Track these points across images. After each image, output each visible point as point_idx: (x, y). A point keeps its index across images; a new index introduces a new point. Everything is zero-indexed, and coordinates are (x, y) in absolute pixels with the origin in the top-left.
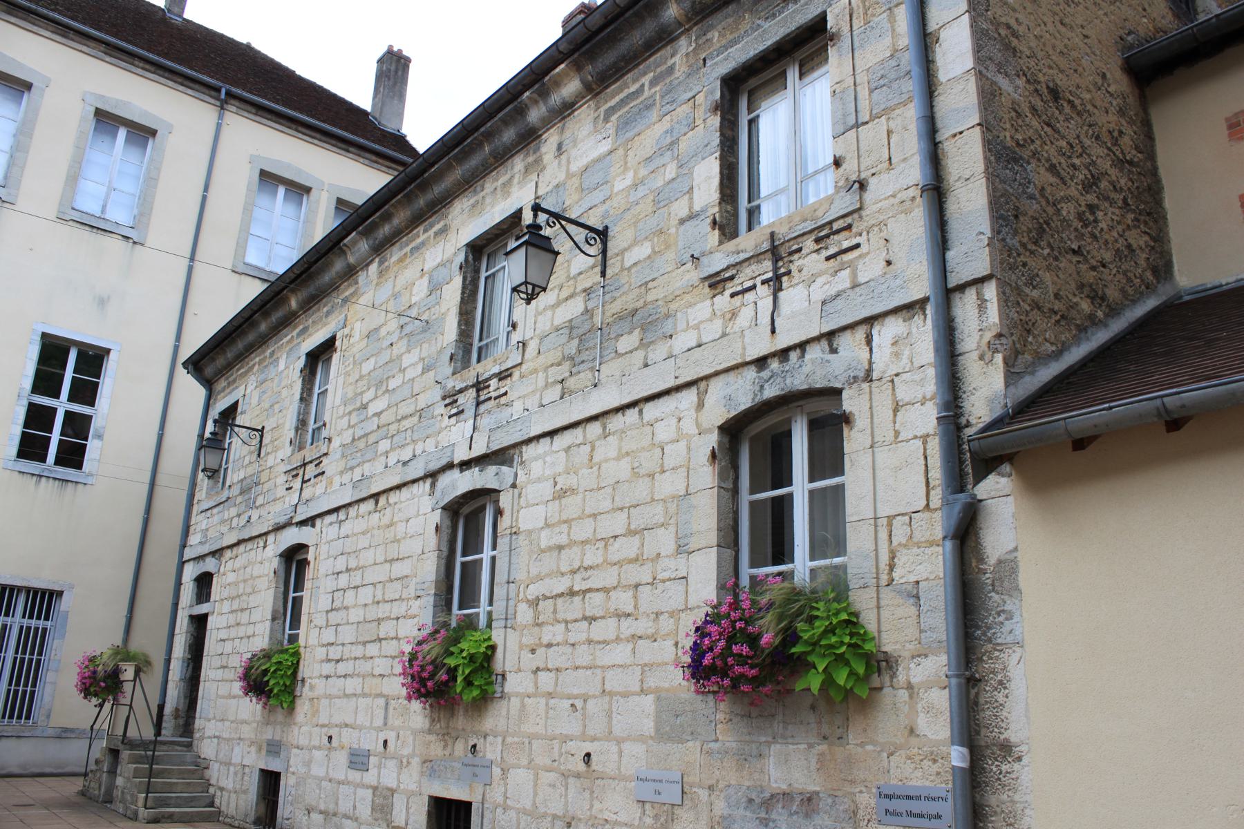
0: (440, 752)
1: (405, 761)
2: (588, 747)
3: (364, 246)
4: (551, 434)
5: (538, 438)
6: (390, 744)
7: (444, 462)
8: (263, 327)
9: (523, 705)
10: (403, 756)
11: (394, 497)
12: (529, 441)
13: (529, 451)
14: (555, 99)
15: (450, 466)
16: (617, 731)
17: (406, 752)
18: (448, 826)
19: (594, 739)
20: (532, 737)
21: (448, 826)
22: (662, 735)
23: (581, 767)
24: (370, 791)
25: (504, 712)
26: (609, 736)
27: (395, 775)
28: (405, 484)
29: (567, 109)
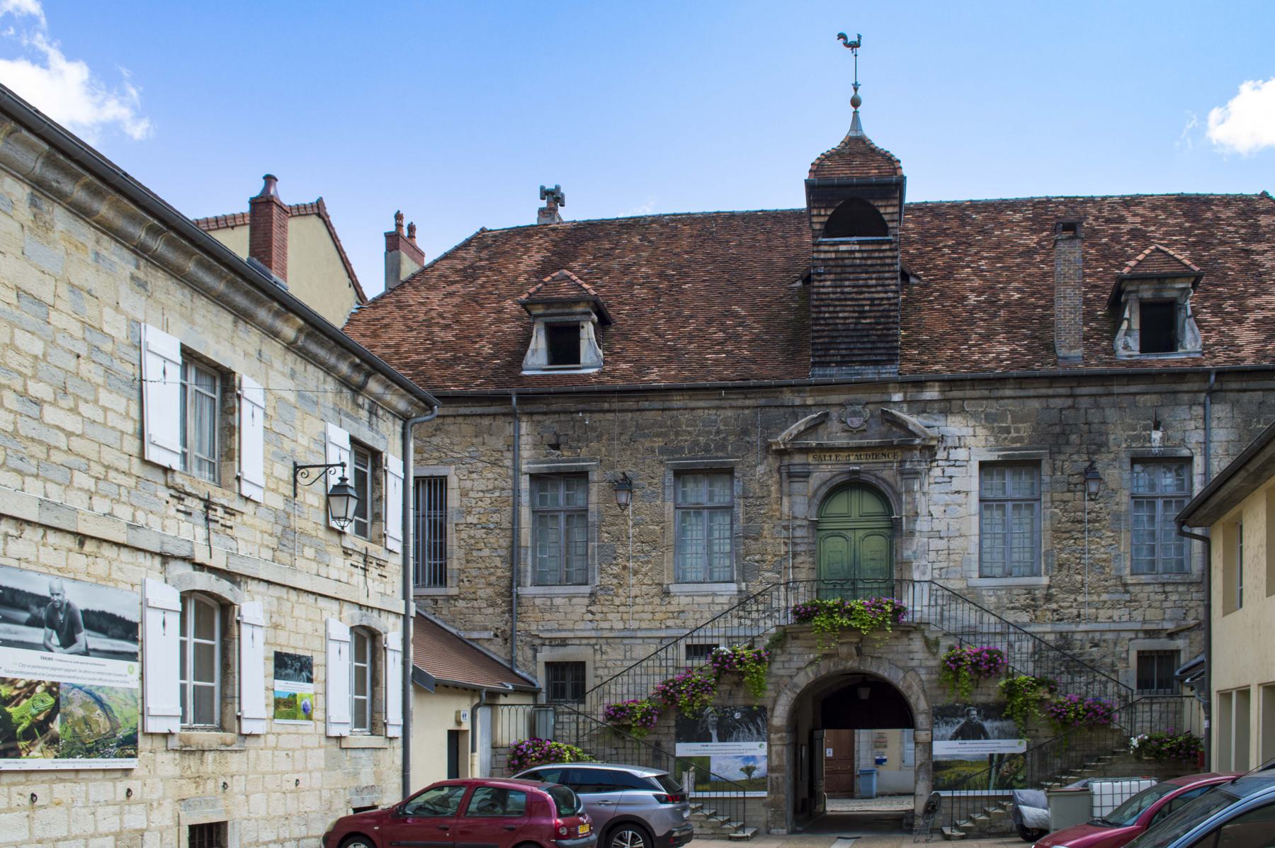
0: (193, 792)
1: (155, 804)
2: (296, 776)
3: (289, 332)
4: (269, 582)
5: (260, 580)
6: (136, 795)
7: (184, 553)
8: (103, 209)
9: (258, 755)
10: (152, 800)
11: (108, 551)
12: (254, 578)
13: (253, 585)
14: (279, 325)
15: (184, 559)
16: (310, 766)
17: (155, 796)
18: (201, 843)
19: (299, 772)
20: (264, 774)
21: (201, 843)
22: (328, 768)
23: (293, 787)
24: (111, 838)
25: (486, 645)
26: (305, 770)
27: (144, 817)
28: (125, 546)
29: (274, 334)
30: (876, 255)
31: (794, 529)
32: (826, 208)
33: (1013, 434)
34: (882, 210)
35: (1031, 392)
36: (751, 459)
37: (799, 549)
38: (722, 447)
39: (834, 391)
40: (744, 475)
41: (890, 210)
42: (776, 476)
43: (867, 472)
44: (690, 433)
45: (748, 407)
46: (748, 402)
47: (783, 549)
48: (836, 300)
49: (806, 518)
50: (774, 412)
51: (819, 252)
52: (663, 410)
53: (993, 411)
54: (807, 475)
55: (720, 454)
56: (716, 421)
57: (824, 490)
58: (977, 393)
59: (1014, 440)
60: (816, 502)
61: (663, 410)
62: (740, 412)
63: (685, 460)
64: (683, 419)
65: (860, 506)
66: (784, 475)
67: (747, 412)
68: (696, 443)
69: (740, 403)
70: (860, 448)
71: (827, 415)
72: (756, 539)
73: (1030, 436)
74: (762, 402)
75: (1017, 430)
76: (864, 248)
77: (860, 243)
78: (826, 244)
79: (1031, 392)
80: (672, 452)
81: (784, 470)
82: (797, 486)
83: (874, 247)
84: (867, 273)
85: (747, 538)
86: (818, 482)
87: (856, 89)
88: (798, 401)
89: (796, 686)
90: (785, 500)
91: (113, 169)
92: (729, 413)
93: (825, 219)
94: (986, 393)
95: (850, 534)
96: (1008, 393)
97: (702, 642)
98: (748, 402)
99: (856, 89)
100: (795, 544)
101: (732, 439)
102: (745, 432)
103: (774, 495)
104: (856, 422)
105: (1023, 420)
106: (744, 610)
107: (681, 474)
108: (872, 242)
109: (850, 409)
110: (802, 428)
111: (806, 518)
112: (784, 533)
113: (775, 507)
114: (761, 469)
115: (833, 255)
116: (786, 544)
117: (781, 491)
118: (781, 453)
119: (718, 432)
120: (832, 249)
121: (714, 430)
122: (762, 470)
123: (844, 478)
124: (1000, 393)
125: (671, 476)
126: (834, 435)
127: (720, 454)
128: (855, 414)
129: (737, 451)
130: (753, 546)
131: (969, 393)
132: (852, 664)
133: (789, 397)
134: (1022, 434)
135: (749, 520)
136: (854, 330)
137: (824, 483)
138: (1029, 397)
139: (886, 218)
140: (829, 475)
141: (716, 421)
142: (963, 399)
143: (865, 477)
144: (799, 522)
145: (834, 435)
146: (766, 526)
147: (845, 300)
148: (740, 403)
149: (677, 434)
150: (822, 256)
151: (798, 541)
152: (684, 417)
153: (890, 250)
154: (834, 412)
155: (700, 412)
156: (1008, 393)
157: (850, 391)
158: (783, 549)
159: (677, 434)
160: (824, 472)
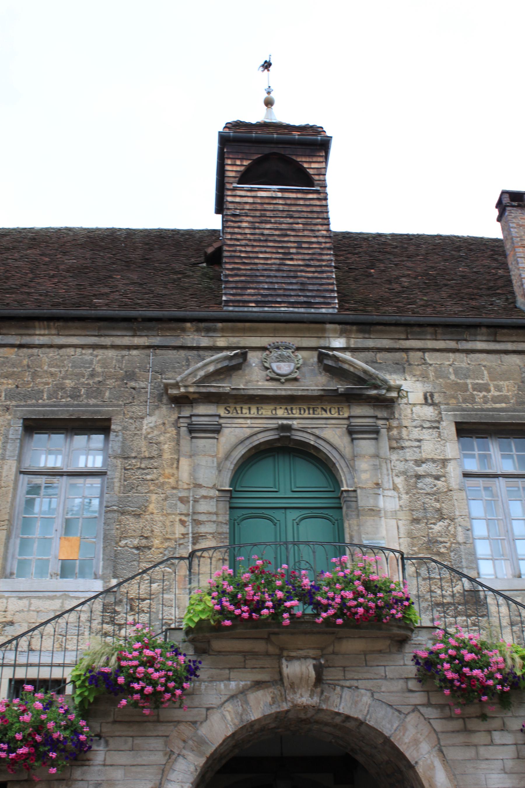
30: (301, 202)
31: (196, 501)
32: (242, 159)
33: (494, 393)
34: (306, 165)
35: (509, 346)
36: (137, 410)
37: (203, 529)
38: (96, 391)
39: (254, 332)
40: (125, 428)
41: (314, 165)
42: (172, 431)
43: (303, 430)
44: (52, 374)
45: (137, 347)
46: (137, 341)
47: (179, 530)
48: (255, 240)
49: (214, 487)
50: (172, 354)
51: (235, 196)
52: (21, 346)
53: (464, 365)
54: (217, 430)
55: (92, 401)
56: (91, 362)
57: (241, 451)
58: (441, 344)
59: (495, 400)
60: (230, 466)
61: (21, 346)
62: (125, 352)
63: (44, 407)
64: (45, 359)
65: (288, 480)
66: (184, 430)
67: (134, 352)
68: (62, 388)
69: (126, 341)
70: (291, 400)
71: (244, 356)
72: (138, 516)
73: (517, 396)
74: (156, 341)
75: (498, 388)
76: (287, 195)
77: (281, 190)
78: (242, 189)
79: (509, 346)
80: (26, 397)
81: (183, 423)
82: (203, 443)
83: (299, 196)
84: (291, 217)
85: (123, 513)
86: (234, 440)
87: (269, 93)
88: (205, 342)
89: (202, 742)
90: (184, 463)
91: (75, 478)
92: (111, 353)
93: (242, 169)
94: (452, 344)
95: (278, 515)
96: (480, 345)
97: (45, 674)
98: (137, 341)
99: (269, 93)
100: (196, 522)
101: (111, 382)
102: (131, 376)
103: (167, 456)
104: (284, 368)
105: (505, 376)
106: (112, 622)
107: (34, 426)
108: (298, 191)
109: (275, 354)
110: (211, 368)
111: (214, 487)
112: (182, 508)
113: (168, 471)
114: (149, 422)
115: (250, 200)
116: (182, 522)
117: (177, 451)
118: (181, 401)
119: (92, 375)
120: (249, 194)
121: (87, 373)
122: (155, 423)
123: (270, 436)
124: (469, 345)
125: (18, 426)
126: (254, 378)
127: (92, 401)
128: (281, 359)
129: (118, 398)
130: (131, 522)
131: (430, 344)
132: (304, 698)
133: (193, 338)
134: (504, 393)
135: (129, 488)
136: (278, 270)
137: (242, 442)
138: (506, 352)
139: (311, 172)
140: (248, 432)
141: (91, 362)
142: (424, 350)
143: (298, 436)
144: (203, 492)
145: (254, 378)
146: (154, 497)
147: (266, 241)
148: (126, 341)
149: (35, 375)
150: (238, 200)
151: (202, 518)
152: (46, 357)
153: (318, 199)
154: (254, 358)
155: (71, 351)
156: (480, 345)
157: (275, 333)
158: (179, 530)
159: (35, 375)
160: (242, 429)
